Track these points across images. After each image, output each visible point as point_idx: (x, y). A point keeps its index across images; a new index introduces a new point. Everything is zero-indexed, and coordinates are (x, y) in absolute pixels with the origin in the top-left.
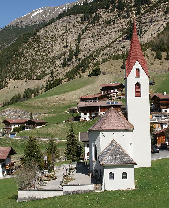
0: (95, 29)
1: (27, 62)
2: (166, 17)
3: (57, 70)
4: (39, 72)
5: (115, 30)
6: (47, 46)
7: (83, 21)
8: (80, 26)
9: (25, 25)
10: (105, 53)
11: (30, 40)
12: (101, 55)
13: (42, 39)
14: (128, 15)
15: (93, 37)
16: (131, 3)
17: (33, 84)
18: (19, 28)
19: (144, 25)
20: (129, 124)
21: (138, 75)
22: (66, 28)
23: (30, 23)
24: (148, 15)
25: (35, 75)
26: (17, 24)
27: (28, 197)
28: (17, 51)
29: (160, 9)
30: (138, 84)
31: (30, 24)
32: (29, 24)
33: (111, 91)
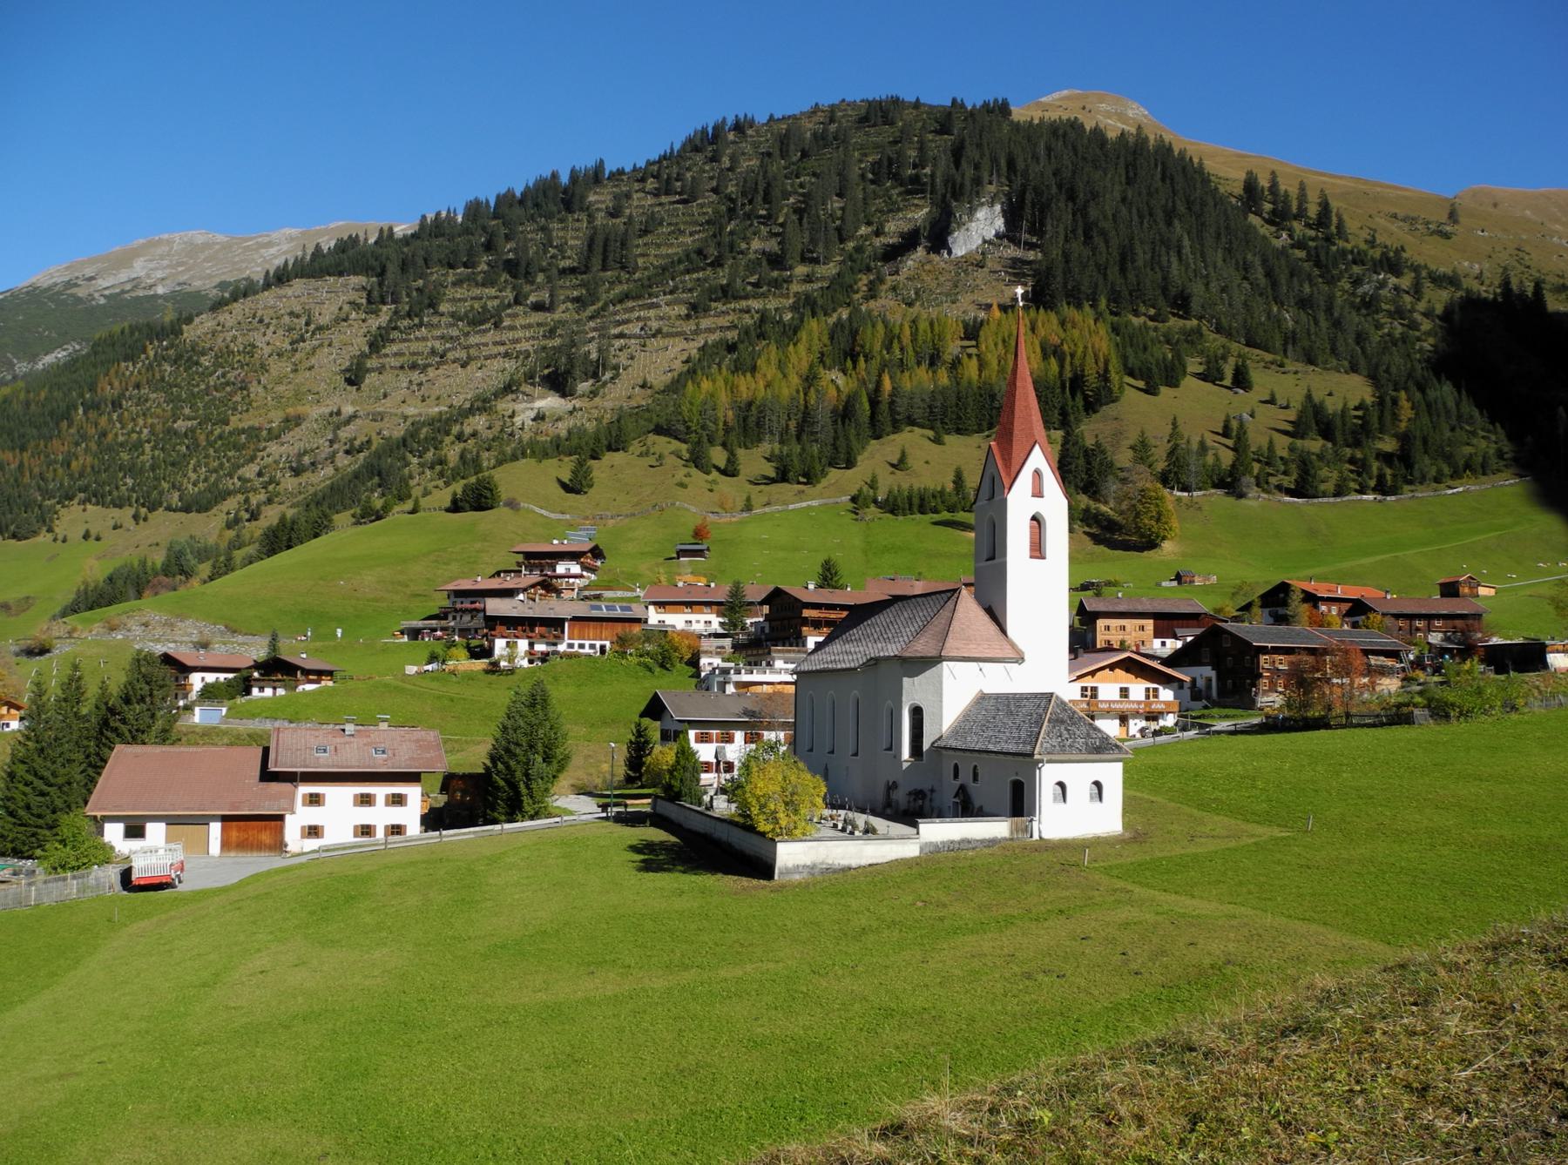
0: (424, 339)
1: (139, 438)
2: (697, 325)
3: (270, 482)
4: (193, 481)
5: (502, 349)
6: (228, 384)
7: (374, 301)
8: (364, 321)
9: (107, 292)
10: (468, 430)
11: (152, 353)
12: (452, 438)
13: (203, 354)
14: (552, 302)
15: (414, 367)
16: (564, 258)
17: (209, 527)
18: (79, 300)
19: (618, 343)
20: (1013, 645)
21: (1038, 493)
22: (307, 324)
23: (128, 287)
24: (632, 309)
25: (176, 495)
26: (70, 284)
27: (809, 863)
28: (92, 389)
29: (671, 292)
30: (1037, 519)
31: (128, 292)
32: (123, 292)
33: (554, 571)
